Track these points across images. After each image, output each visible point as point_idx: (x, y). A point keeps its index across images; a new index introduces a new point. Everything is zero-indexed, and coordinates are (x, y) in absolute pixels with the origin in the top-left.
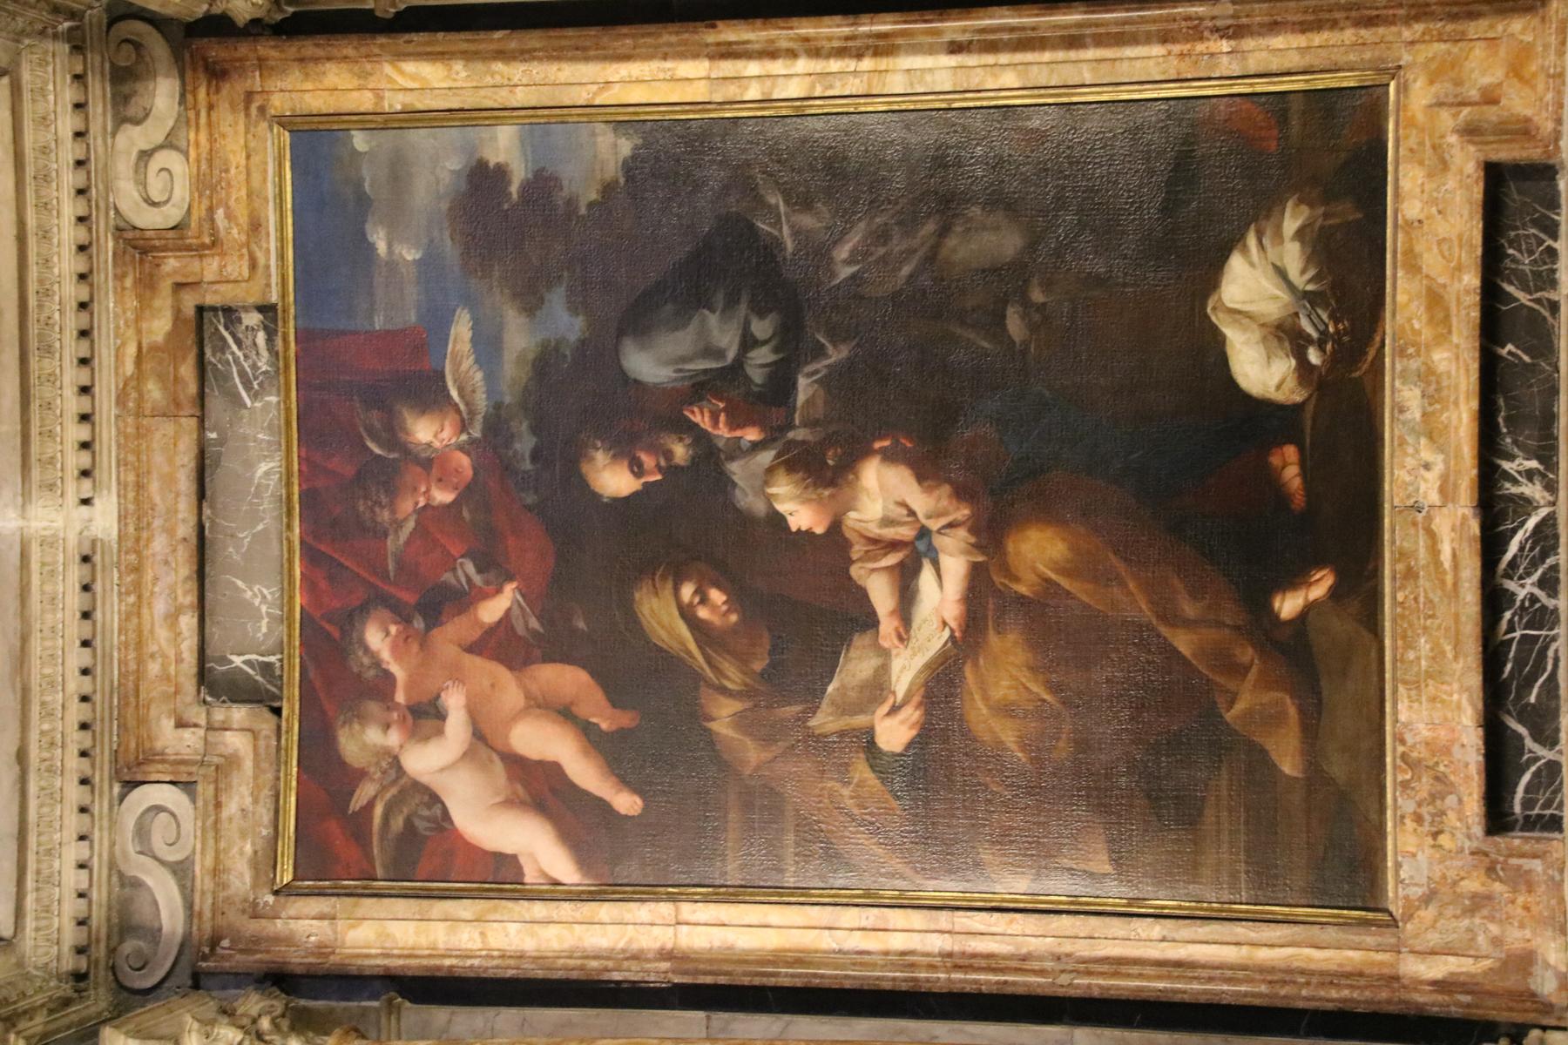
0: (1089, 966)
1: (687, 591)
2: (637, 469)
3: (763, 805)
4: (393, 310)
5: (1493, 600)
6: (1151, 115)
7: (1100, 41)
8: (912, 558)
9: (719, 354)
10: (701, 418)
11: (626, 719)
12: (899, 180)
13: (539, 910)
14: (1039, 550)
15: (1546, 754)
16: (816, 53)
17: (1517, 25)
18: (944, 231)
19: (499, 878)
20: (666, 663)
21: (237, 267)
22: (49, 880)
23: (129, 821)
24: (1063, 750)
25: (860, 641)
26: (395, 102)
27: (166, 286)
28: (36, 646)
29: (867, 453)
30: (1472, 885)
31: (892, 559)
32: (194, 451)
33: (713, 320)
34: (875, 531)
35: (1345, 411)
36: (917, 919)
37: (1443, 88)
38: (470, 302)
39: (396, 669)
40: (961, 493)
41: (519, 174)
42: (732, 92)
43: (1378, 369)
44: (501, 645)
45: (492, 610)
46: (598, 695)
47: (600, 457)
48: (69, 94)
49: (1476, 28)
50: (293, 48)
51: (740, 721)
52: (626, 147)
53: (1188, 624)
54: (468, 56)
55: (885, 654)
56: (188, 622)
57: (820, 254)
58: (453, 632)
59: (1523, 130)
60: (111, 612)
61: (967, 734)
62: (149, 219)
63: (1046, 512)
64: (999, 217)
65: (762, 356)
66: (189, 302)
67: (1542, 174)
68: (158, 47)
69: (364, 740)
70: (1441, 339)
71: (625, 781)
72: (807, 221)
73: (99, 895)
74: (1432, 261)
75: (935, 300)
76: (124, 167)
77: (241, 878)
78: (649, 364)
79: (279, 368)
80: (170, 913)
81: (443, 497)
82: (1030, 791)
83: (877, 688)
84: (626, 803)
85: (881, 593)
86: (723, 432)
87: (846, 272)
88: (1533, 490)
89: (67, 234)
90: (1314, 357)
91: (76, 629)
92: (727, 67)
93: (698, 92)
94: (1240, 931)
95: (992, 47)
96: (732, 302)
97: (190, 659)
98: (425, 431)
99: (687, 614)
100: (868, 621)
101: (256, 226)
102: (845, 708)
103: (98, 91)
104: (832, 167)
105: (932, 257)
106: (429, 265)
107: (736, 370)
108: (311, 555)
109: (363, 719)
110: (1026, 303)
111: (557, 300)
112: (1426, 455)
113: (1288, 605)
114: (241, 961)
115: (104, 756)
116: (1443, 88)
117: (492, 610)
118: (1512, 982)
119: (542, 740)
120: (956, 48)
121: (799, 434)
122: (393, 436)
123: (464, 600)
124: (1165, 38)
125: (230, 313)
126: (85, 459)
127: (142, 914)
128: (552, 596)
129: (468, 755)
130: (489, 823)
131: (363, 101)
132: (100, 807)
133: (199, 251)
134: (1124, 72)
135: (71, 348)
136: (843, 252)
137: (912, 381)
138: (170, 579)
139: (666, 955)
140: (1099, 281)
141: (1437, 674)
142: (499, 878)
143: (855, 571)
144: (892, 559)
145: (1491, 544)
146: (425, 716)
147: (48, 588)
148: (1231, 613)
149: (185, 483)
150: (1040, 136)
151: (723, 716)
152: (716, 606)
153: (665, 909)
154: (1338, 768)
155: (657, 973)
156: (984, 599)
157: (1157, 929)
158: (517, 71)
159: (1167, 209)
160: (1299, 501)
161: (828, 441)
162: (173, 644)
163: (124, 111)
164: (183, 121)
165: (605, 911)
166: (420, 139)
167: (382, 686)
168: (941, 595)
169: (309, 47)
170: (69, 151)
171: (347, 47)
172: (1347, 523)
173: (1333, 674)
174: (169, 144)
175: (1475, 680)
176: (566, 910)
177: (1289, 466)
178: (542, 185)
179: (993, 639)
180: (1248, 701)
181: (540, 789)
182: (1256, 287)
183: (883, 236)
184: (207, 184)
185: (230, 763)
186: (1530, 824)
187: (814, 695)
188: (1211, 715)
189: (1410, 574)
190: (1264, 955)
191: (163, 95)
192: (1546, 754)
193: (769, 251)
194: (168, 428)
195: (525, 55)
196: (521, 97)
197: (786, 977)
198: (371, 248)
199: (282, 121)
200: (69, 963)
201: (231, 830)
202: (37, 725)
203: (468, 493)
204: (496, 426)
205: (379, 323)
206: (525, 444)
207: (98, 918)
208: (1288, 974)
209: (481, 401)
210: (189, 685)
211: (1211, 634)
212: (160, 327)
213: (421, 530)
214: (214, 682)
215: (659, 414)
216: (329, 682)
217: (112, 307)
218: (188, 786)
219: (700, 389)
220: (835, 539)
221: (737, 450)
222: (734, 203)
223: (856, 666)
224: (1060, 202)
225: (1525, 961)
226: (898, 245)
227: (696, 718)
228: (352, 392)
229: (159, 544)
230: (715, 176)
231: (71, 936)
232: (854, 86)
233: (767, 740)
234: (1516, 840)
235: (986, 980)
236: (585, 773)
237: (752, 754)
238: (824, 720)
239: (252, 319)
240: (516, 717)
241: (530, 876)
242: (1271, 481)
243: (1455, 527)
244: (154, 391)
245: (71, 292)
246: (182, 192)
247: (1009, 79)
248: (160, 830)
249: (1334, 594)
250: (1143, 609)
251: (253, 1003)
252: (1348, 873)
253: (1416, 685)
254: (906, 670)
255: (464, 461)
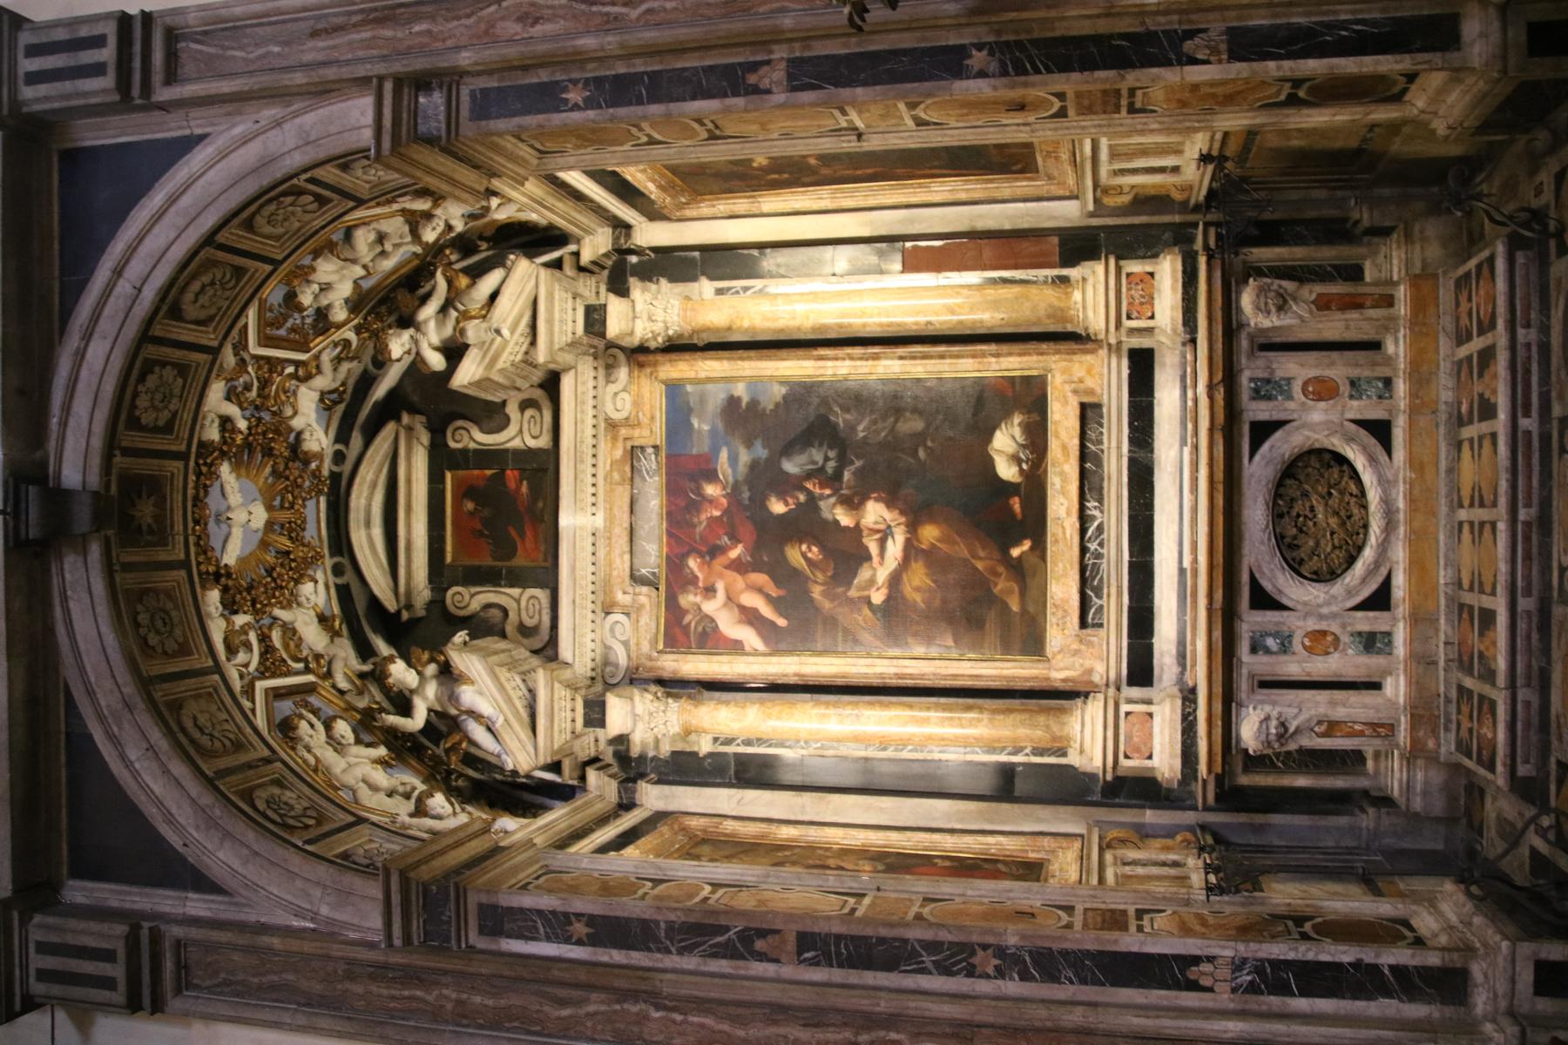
0: (945, 677)
1: (804, 547)
2: (787, 504)
3: (831, 623)
4: (699, 447)
5: (1083, 550)
6: (968, 382)
7: (951, 357)
8: (884, 536)
9: (814, 463)
10: (809, 485)
11: (781, 593)
12: (881, 403)
13: (751, 659)
14: (930, 533)
15: (1099, 602)
16: (852, 358)
17: (1089, 358)
18: (897, 421)
19: (736, 648)
20: (795, 573)
21: (646, 433)
22: (582, 645)
23: (607, 627)
24: (937, 603)
25: (866, 565)
26: (703, 375)
27: (621, 439)
28: (578, 564)
29: (869, 498)
30: (1075, 646)
31: (878, 536)
32: (627, 500)
33: (814, 451)
34: (872, 526)
35: (1034, 486)
36: (886, 662)
37: (1065, 377)
38: (727, 444)
39: (700, 575)
40: (902, 513)
41: (745, 400)
42: (821, 372)
43: (1046, 471)
44: (738, 567)
45: (734, 554)
46: (772, 584)
47: (773, 499)
48: (592, 374)
49: (1076, 358)
50: (668, 357)
51: (825, 594)
52: (784, 390)
53: (980, 559)
54: (729, 359)
55: (875, 569)
56: (627, 557)
57: (852, 428)
58: (720, 562)
59: (1091, 392)
60: (601, 553)
61: (903, 598)
62: (616, 416)
63: (932, 519)
64: (916, 416)
65: (831, 465)
66: (629, 444)
67: (1098, 406)
68: (621, 357)
69: (688, 599)
70: (1067, 461)
71: (781, 615)
72: (848, 416)
73: (598, 651)
74: (1064, 435)
75: (893, 445)
76: (608, 398)
77: (646, 647)
78: (791, 467)
79: (659, 468)
80: (622, 660)
81: (717, 513)
82: (927, 617)
83: (872, 582)
84: (782, 622)
85: (873, 548)
86: (817, 491)
87: (861, 435)
88: (1096, 513)
89: (590, 421)
90: (1025, 466)
91: (590, 559)
92: (821, 363)
93: (810, 372)
94: (997, 664)
95: (914, 358)
96: (821, 445)
97: (628, 570)
98: (711, 490)
99: (804, 555)
100: (869, 558)
101: (653, 418)
102: (861, 589)
103: (601, 372)
104: (857, 399)
105: (893, 429)
106: (713, 433)
107: (822, 469)
108: (670, 534)
109: (688, 592)
110: (926, 447)
111: (758, 444)
112: (1062, 500)
113: (1015, 552)
114: (646, 675)
115: (599, 604)
116: (1065, 377)
117: (734, 554)
118: (1085, 678)
119: (752, 600)
120: (901, 358)
121: (844, 492)
122: (699, 491)
123: (723, 550)
124: (974, 356)
125: (642, 448)
126: (593, 499)
127: (612, 659)
128: (756, 549)
129: (725, 605)
130: (730, 627)
131: (692, 375)
132: (598, 621)
133: (633, 426)
134: (960, 368)
135: (590, 461)
136: (860, 428)
137: (887, 473)
138: (622, 542)
139: (796, 675)
140: (951, 439)
141: (1065, 575)
142: (736, 648)
143: (865, 540)
144: (878, 536)
145: (1083, 531)
146: (710, 591)
147: (203, 568)
148: (997, 555)
149: (626, 508)
150: (929, 389)
151: (817, 592)
152: (815, 552)
153: (796, 659)
154: (1031, 609)
155: (792, 680)
156: (910, 550)
157: (969, 664)
158: (746, 364)
159: (974, 415)
160: (1019, 516)
161: (855, 494)
162: (622, 565)
163: (609, 380)
164: (630, 382)
165: (774, 659)
166: (710, 387)
167: (694, 580)
168: (895, 548)
169: (673, 356)
170: (591, 393)
171: (687, 356)
172: (1035, 525)
173: (1029, 575)
174: (624, 390)
175: (1077, 577)
176: (761, 659)
177: (1016, 504)
178: (754, 403)
179: (914, 565)
180: (1003, 585)
181: (750, 617)
182: (1005, 442)
183: (874, 422)
184: (637, 404)
185: (640, 608)
186: (1094, 625)
187: (849, 584)
188: (989, 590)
189: (1056, 541)
190: (1005, 672)
191: (623, 373)
192: (1099, 602)
193: (835, 426)
194: (620, 488)
195: (749, 359)
196: (747, 373)
197: (840, 682)
198: (691, 425)
199: (663, 382)
200: (590, 674)
201: (642, 630)
202: (579, 592)
203: (725, 512)
204: (736, 486)
205: (695, 451)
206: (746, 495)
207: (598, 659)
208: (1014, 678)
209: (731, 479)
210: (627, 579)
211: (988, 562)
212: (619, 453)
213: (709, 525)
214: (636, 579)
215: (796, 484)
216: (676, 579)
217: (604, 446)
218: (627, 614)
219: (809, 475)
220: (857, 530)
221: (822, 497)
222: (822, 411)
223: (864, 574)
224: (938, 412)
225: (1090, 671)
226: (880, 425)
227: (807, 592)
228: (686, 475)
229: (617, 530)
230: (815, 401)
231: (590, 665)
232: (866, 370)
233: (832, 600)
234: (1089, 631)
235: (910, 683)
236: (767, 611)
237: (827, 605)
238: (853, 593)
239: (650, 450)
240: (742, 592)
241: (747, 648)
242: (1010, 509)
243: (1072, 524)
244: (616, 476)
245: (590, 441)
246: (628, 406)
247: (920, 369)
248: (618, 628)
249: (1032, 549)
250: (965, 554)
251: (653, 688)
252: (1034, 644)
253: (1058, 579)
254: (882, 575)
255: (724, 501)
